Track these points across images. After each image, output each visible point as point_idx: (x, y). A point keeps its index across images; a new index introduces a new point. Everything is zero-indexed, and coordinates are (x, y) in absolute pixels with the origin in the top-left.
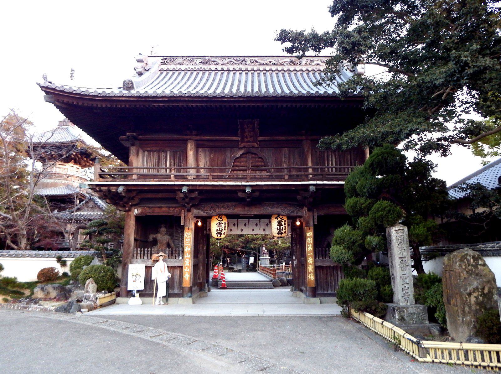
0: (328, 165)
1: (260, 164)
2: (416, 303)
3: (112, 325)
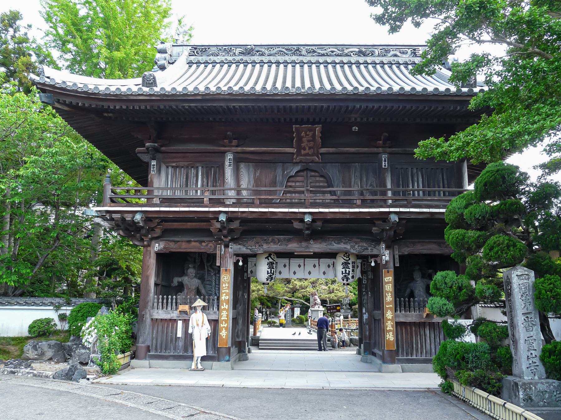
0: (413, 187)
1: (321, 184)
2: (548, 378)
3: (129, 399)
